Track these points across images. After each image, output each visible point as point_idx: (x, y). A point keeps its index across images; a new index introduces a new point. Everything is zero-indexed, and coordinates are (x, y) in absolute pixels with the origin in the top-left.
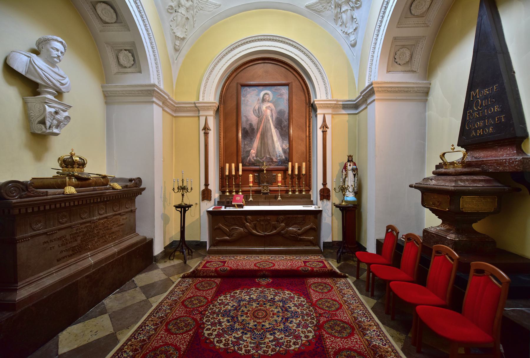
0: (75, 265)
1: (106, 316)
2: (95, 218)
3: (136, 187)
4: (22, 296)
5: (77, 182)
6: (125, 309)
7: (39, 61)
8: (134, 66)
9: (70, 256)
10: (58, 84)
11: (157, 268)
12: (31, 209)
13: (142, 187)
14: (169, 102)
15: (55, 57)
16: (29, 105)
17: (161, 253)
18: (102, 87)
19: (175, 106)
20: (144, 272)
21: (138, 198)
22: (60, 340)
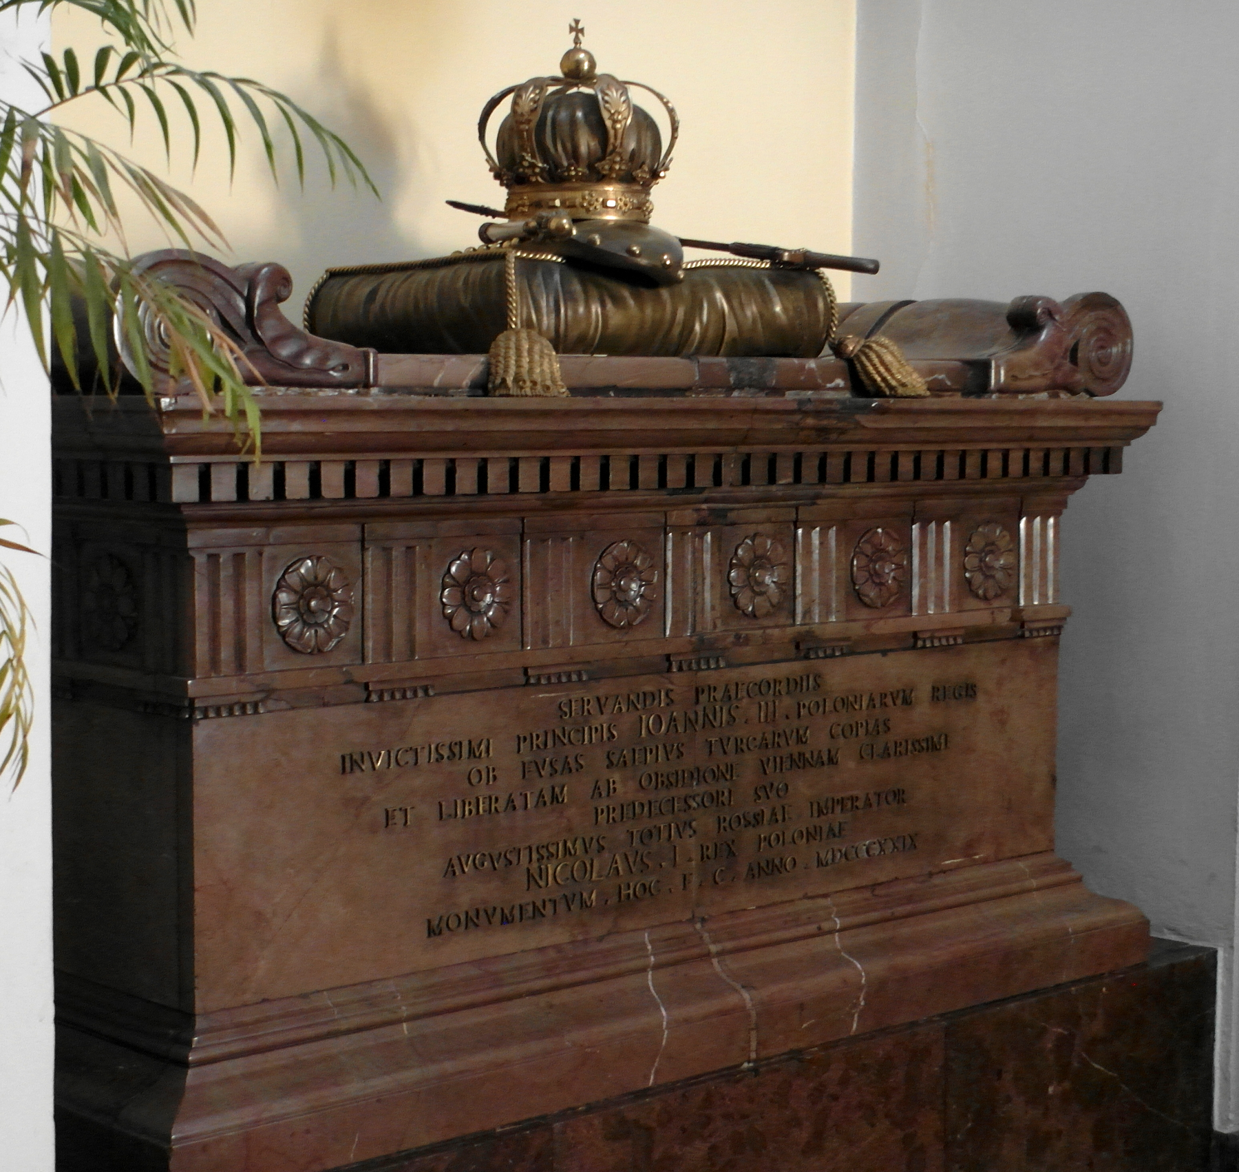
13: (1130, 392)
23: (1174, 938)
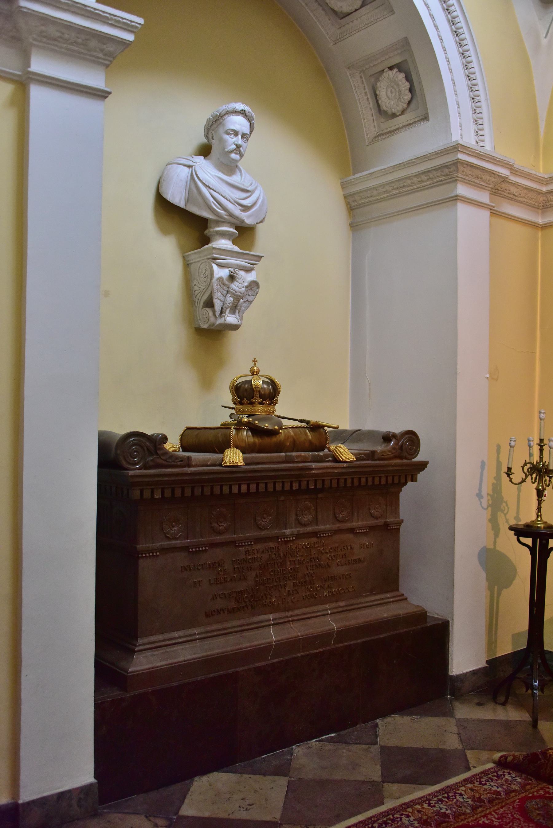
0: (238, 635)
1: (283, 781)
2: (288, 531)
3: (401, 458)
4: (139, 668)
5: (251, 440)
6: (322, 784)
7: (207, 170)
8: (413, 105)
9: (232, 611)
10: (236, 211)
11: (449, 714)
12: (160, 491)
13: (419, 458)
14: (516, 185)
15: (231, 152)
16: (192, 267)
17: (474, 672)
18: (343, 186)
19: (539, 193)
20: (411, 714)
21: (408, 493)
22: (192, 789)
23: (437, 616)
